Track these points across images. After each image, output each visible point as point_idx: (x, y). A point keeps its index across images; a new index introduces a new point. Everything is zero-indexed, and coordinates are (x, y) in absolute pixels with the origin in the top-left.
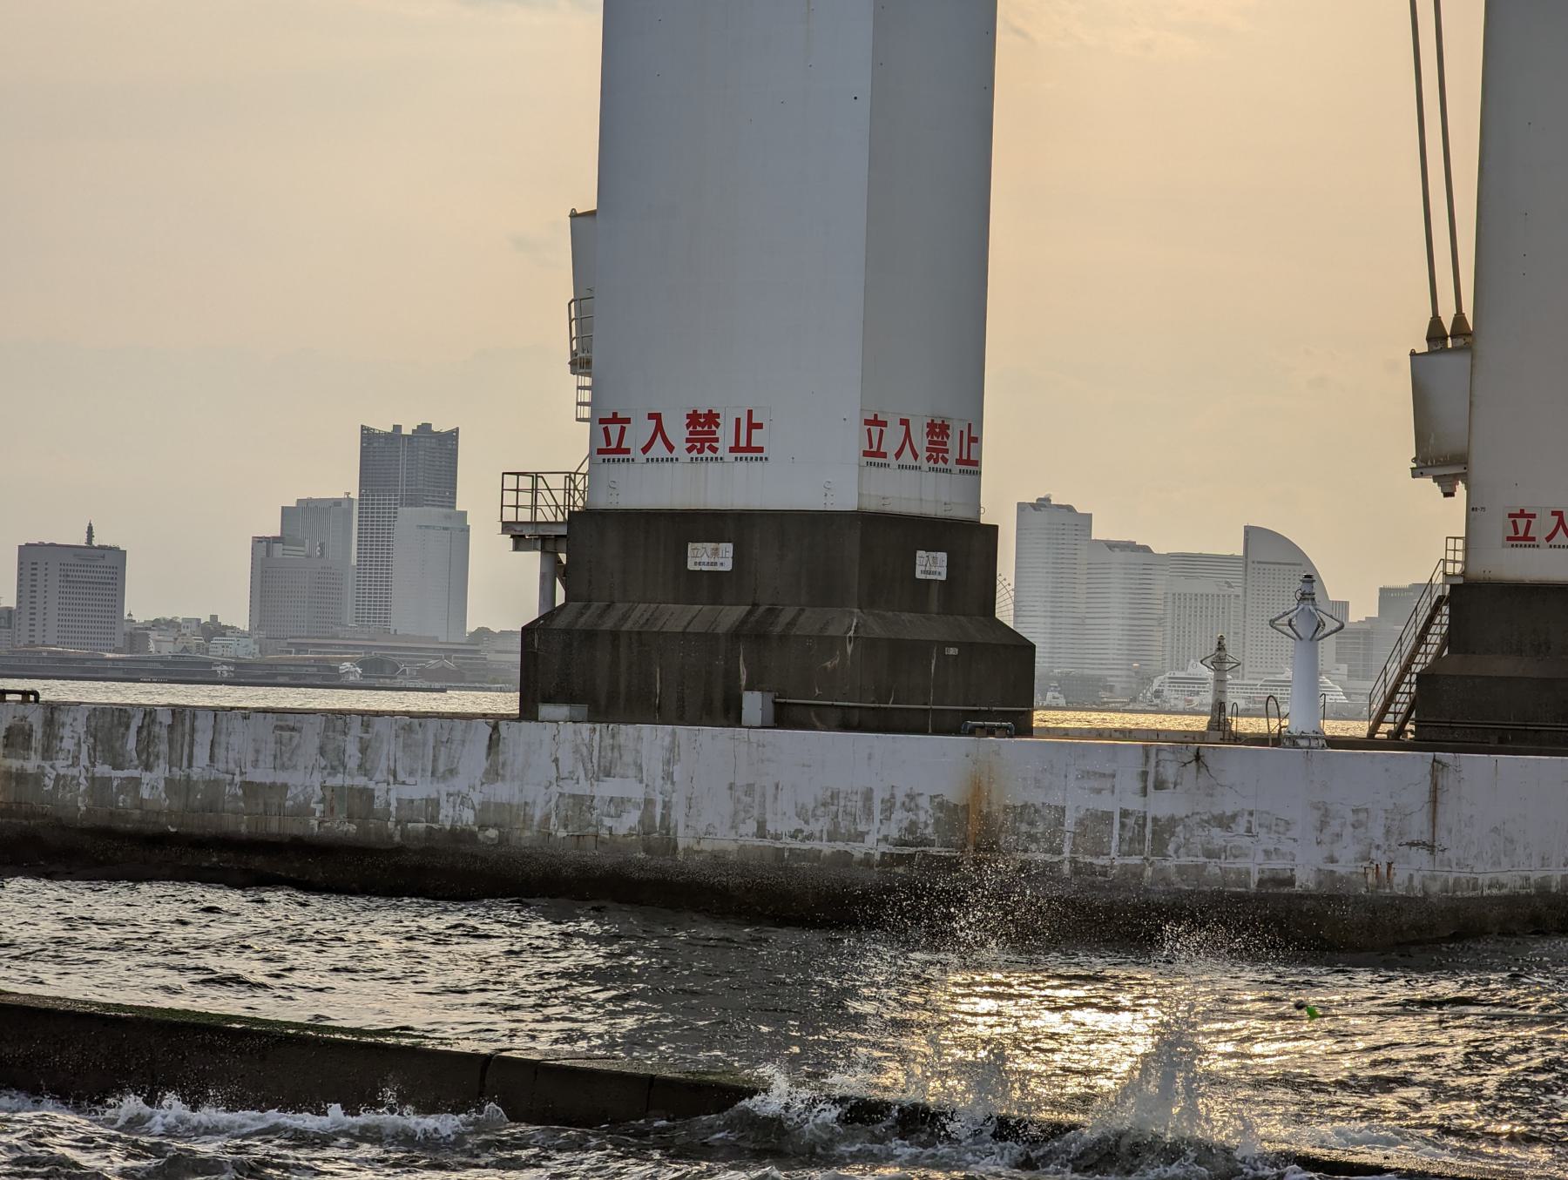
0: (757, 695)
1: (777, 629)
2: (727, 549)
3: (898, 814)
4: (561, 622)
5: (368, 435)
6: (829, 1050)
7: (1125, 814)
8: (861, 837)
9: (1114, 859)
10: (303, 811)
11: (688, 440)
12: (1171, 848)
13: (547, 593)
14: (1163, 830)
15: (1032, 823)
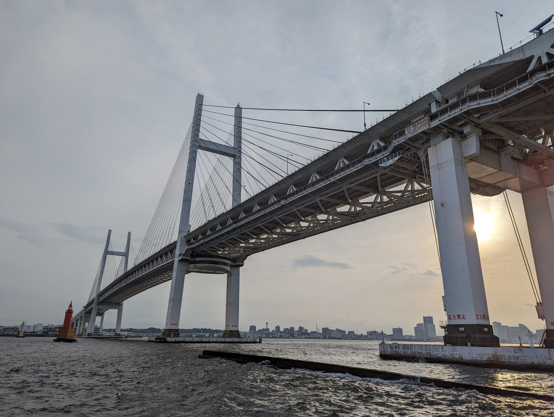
0: (469, 343)
1: (470, 336)
2: (463, 328)
3: (487, 356)
4: (447, 336)
5: (424, 317)
7: (513, 356)
8: (483, 358)
9: (512, 360)
10: (424, 355)
12: (519, 359)
13: (445, 333)
14: (518, 357)
15: (502, 357)
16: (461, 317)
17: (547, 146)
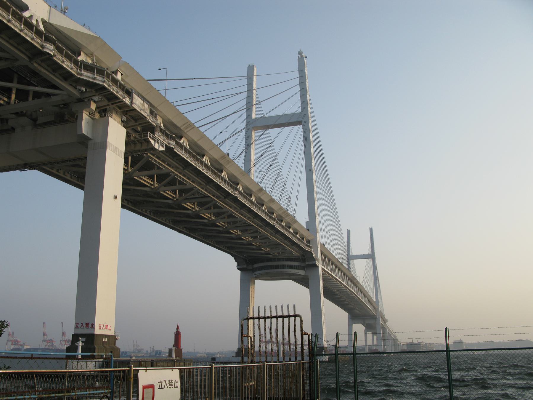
6: (406, 367)
16: (90, 326)
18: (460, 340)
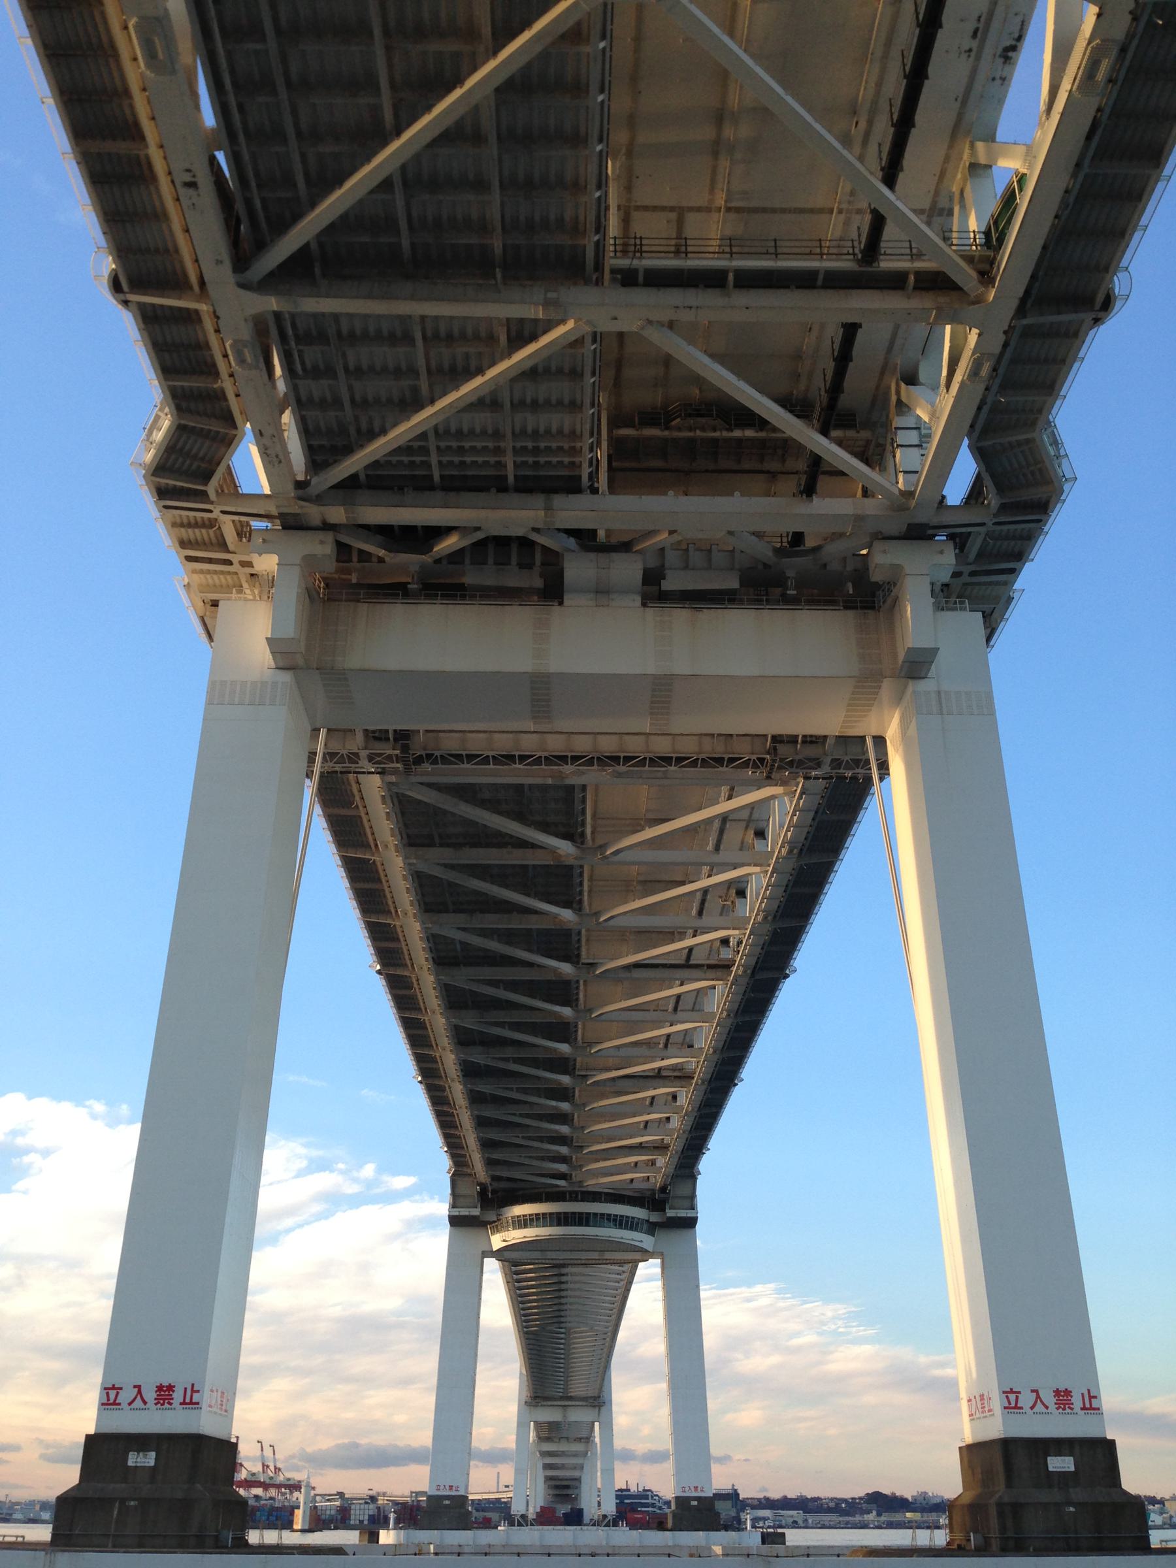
11: (1056, 1404)
17: (784, 858)
18: (730, 1487)
